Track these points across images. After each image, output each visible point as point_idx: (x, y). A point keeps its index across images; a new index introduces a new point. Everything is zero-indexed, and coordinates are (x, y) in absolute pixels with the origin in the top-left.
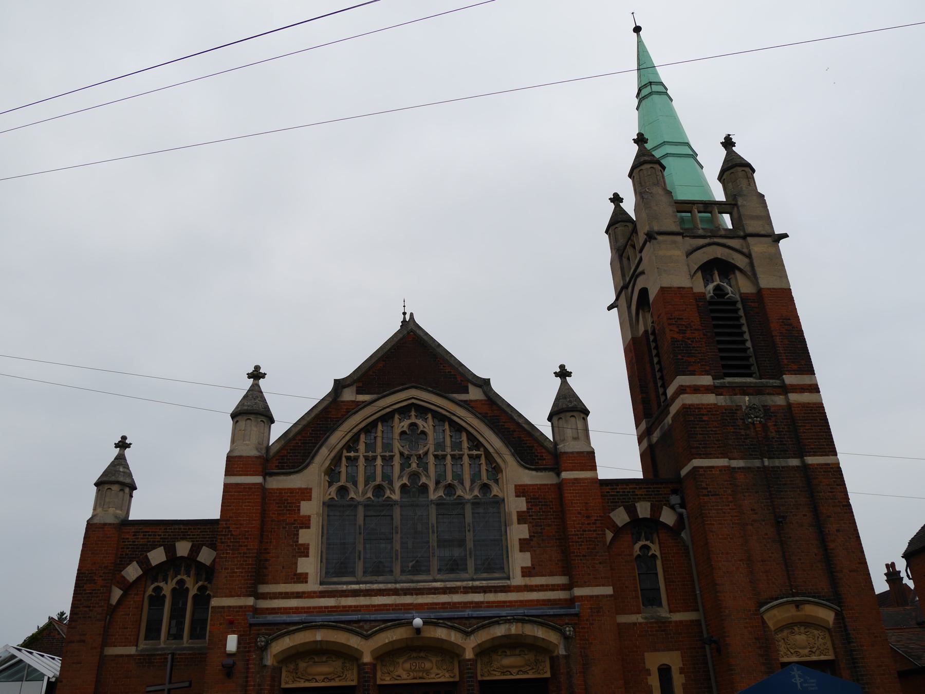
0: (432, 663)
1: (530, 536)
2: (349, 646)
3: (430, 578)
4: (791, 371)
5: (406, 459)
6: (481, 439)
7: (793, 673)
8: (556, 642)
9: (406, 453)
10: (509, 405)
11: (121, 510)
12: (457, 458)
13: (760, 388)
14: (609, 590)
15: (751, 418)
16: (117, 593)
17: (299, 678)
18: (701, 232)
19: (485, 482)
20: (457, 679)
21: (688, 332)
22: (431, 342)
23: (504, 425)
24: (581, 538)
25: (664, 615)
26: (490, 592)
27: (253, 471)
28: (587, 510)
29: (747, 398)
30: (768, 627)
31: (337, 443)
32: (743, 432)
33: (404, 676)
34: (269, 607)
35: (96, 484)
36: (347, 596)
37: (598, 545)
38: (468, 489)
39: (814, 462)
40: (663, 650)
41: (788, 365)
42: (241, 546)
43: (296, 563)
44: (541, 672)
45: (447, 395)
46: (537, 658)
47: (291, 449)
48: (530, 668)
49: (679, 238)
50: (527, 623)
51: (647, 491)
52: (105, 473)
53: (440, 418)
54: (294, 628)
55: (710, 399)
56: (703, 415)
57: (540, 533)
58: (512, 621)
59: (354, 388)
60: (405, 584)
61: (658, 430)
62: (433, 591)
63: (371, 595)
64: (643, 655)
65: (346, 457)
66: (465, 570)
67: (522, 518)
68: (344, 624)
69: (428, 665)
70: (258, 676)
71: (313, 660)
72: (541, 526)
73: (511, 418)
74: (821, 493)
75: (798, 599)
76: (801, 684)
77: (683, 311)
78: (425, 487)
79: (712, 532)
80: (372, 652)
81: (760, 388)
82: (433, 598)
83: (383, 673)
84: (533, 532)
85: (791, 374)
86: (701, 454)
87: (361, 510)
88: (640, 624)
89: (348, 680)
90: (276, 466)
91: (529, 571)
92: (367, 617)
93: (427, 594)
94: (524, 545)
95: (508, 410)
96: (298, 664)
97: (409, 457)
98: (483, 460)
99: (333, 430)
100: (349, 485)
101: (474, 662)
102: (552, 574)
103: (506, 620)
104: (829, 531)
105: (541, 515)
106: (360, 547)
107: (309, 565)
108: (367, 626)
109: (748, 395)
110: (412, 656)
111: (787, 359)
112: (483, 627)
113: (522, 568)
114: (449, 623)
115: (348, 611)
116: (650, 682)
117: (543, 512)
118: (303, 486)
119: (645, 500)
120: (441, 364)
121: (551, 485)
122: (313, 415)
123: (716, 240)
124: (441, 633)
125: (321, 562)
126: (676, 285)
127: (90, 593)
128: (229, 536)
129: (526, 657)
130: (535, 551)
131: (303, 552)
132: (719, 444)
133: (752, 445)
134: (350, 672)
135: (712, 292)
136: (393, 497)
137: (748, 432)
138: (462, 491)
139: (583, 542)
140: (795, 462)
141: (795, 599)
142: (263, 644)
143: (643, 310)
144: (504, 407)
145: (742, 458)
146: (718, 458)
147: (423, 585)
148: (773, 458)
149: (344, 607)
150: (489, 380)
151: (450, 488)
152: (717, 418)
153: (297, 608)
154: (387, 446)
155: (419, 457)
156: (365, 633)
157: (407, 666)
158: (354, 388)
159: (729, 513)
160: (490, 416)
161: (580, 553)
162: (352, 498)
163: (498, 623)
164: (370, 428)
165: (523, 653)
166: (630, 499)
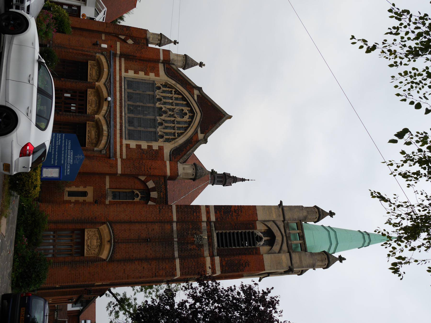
0: (95, 108)
1: (142, 149)
3: (126, 113)
4: (222, 261)
5: (172, 110)
6: (182, 136)
7: (81, 156)
8: (100, 147)
9: (175, 110)
11: (152, 40)
12: (173, 128)
13: (212, 245)
14: (119, 172)
15: (196, 236)
16: (123, 37)
18: (288, 231)
21: (235, 214)
25: (108, 198)
26: (120, 132)
29: (206, 238)
30: (101, 226)
32: (190, 232)
33: (90, 98)
35: (161, 34)
38: (162, 130)
39: (176, 262)
40: (94, 195)
41: (225, 260)
42: (138, 51)
45: (199, 125)
49: (282, 219)
51: (162, 197)
52: (165, 37)
53: (190, 123)
54: (109, 62)
55: (204, 218)
56: (196, 213)
59: (199, 94)
63: (120, 92)
64: (92, 186)
66: (129, 126)
67: (150, 147)
69: (93, 106)
72: (147, 154)
74: (162, 263)
75: (112, 241)
76: (77, 158)
77: (246, 214)
79: (143, 207)
80: (99, 86)
81: (212, 245)
84: (144, 151)
85: (220, 261)
86: (178, 209)
87: (151, 93)
88: (105, 187)
92: (112, 85)
94: (139, 146)
99: (182, 86)
100: (161, 90)
104: (143, 263)
105: (151, 154)
106: (138, 92)
107: (131, 73)
108: (108, 84)
109: (208, 238)
111: (228, 260)
112: (107, 122)
114: (108, 110)
115: (114, 84)
116: (81, 187)
117: (152, 155)
118: (160, 75)
119: (158, 196)
122: (187, 79)
123: (285, 238)
124: (105, 108)
126: (258, 212)
127: (123, 30)
129: (94, 140)
131: (136, 72)
132: (183, 218)
133: (184, 235)
135: (258, 234)
137: (190, 235)
139: (140, 165)
140: (176, 254)
141: (112, 240)
145: (177, 229)
146: (177, 216)
148: (178, 245)
149: (116, 83)
151: (161, 124)
152: (195, 220)
153: (116, 69)
154: (177, 105)
155: (173, 115)
156: (106, 83)
157: (94, 99)
158: (199, 94)
159: (152, 216)
162: (156, 91)
164: (184, 99)
166: (159, 190)
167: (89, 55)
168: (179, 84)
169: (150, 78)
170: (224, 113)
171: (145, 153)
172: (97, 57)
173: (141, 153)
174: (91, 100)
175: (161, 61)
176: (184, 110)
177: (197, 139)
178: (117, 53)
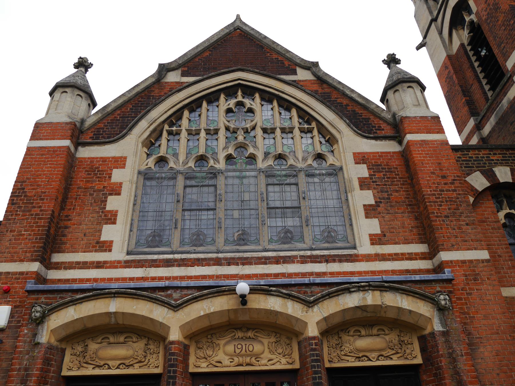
0: (263, 344)
1: (376, 202)
2: (152, 320)
3: (260, 248)
8: (428, 314)
9: (232, 126)
10: (340, 83)
14: (484, 255)
17: (86, 363)
19: (319, 152)
20: (297, 366)
22: (258, 35)
23: (336, 101)
24: (439, 198)
26: (334, 261)
27: (61, 136)
28: (441, 170)
31: (158, 116)
33: (226, 361)
34: (62, 278)
36: (158, 266)
37: (461, 205)
42: (34, 207)
43: (100, 231)
44: (408, 357)
46: (402, 339)
47: (108, 123)
48: (394, 352)
50: (387, 291)
57: (387, 198)
58: (367, 288)
59: (179, 72)
60: (229, 254)
61: (493, 116)
62: (263, 260)
65: (167, 131)
68: (148, 292)
69: (257, 348)
70: (27, 356)
71: (108, 341)
72: (387, 192)
73: (344, 95)
78: (252, 158)
80: (182, 328)
82: (263, 268)
83: (197, 358)
89: (151, 366)
90: (90, 138)
91: (380, 239)
93: (255, 264)
95: (339, 86)
96: (87, 345)
97: (235, 132)
98: (315, 132)
99: (156, 105)
101: (319, 341)
102: (407, 242)
103: (359, 287)
108: (176, 295)
110: (237, 337)
112: (330, 296)
113: (370, 235)
114: (284, 291)
120: (268, 52)
121: (394, 153)
122: (134, 92)
125: (131, 231)
128: (22, 198)
129: (387, 338)
130: (383, 217)
131: (110, 219)
134: (155, 356)
136: (217, 166)
138: (294, 161)
139: (442, 202)
142: (38, 315)
143: (456, 29)
144: (335, 84)
147: (251, 255)
150: (317, 63)
157: (230, 348)
158: (179, 72)
160: (321, 93)
161: (441, 213)
163: (348, 291)
165: (383, 333)
166: (485, 163)
167: (42, 370)
168: (149, 111)
169: (131, 182)
170: (232, 28)
171: (385, 195)
172: (53, 341)
173: (391, 206)
174: (236, 359)
175: (72, 149)
176: (231, 106)
177: (314, 84)
178: (35, 270)
